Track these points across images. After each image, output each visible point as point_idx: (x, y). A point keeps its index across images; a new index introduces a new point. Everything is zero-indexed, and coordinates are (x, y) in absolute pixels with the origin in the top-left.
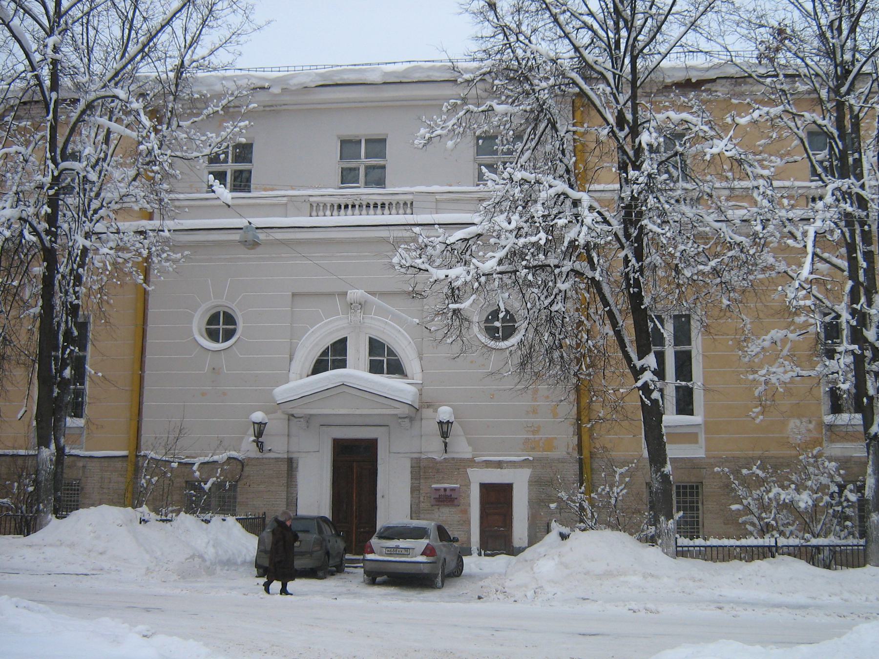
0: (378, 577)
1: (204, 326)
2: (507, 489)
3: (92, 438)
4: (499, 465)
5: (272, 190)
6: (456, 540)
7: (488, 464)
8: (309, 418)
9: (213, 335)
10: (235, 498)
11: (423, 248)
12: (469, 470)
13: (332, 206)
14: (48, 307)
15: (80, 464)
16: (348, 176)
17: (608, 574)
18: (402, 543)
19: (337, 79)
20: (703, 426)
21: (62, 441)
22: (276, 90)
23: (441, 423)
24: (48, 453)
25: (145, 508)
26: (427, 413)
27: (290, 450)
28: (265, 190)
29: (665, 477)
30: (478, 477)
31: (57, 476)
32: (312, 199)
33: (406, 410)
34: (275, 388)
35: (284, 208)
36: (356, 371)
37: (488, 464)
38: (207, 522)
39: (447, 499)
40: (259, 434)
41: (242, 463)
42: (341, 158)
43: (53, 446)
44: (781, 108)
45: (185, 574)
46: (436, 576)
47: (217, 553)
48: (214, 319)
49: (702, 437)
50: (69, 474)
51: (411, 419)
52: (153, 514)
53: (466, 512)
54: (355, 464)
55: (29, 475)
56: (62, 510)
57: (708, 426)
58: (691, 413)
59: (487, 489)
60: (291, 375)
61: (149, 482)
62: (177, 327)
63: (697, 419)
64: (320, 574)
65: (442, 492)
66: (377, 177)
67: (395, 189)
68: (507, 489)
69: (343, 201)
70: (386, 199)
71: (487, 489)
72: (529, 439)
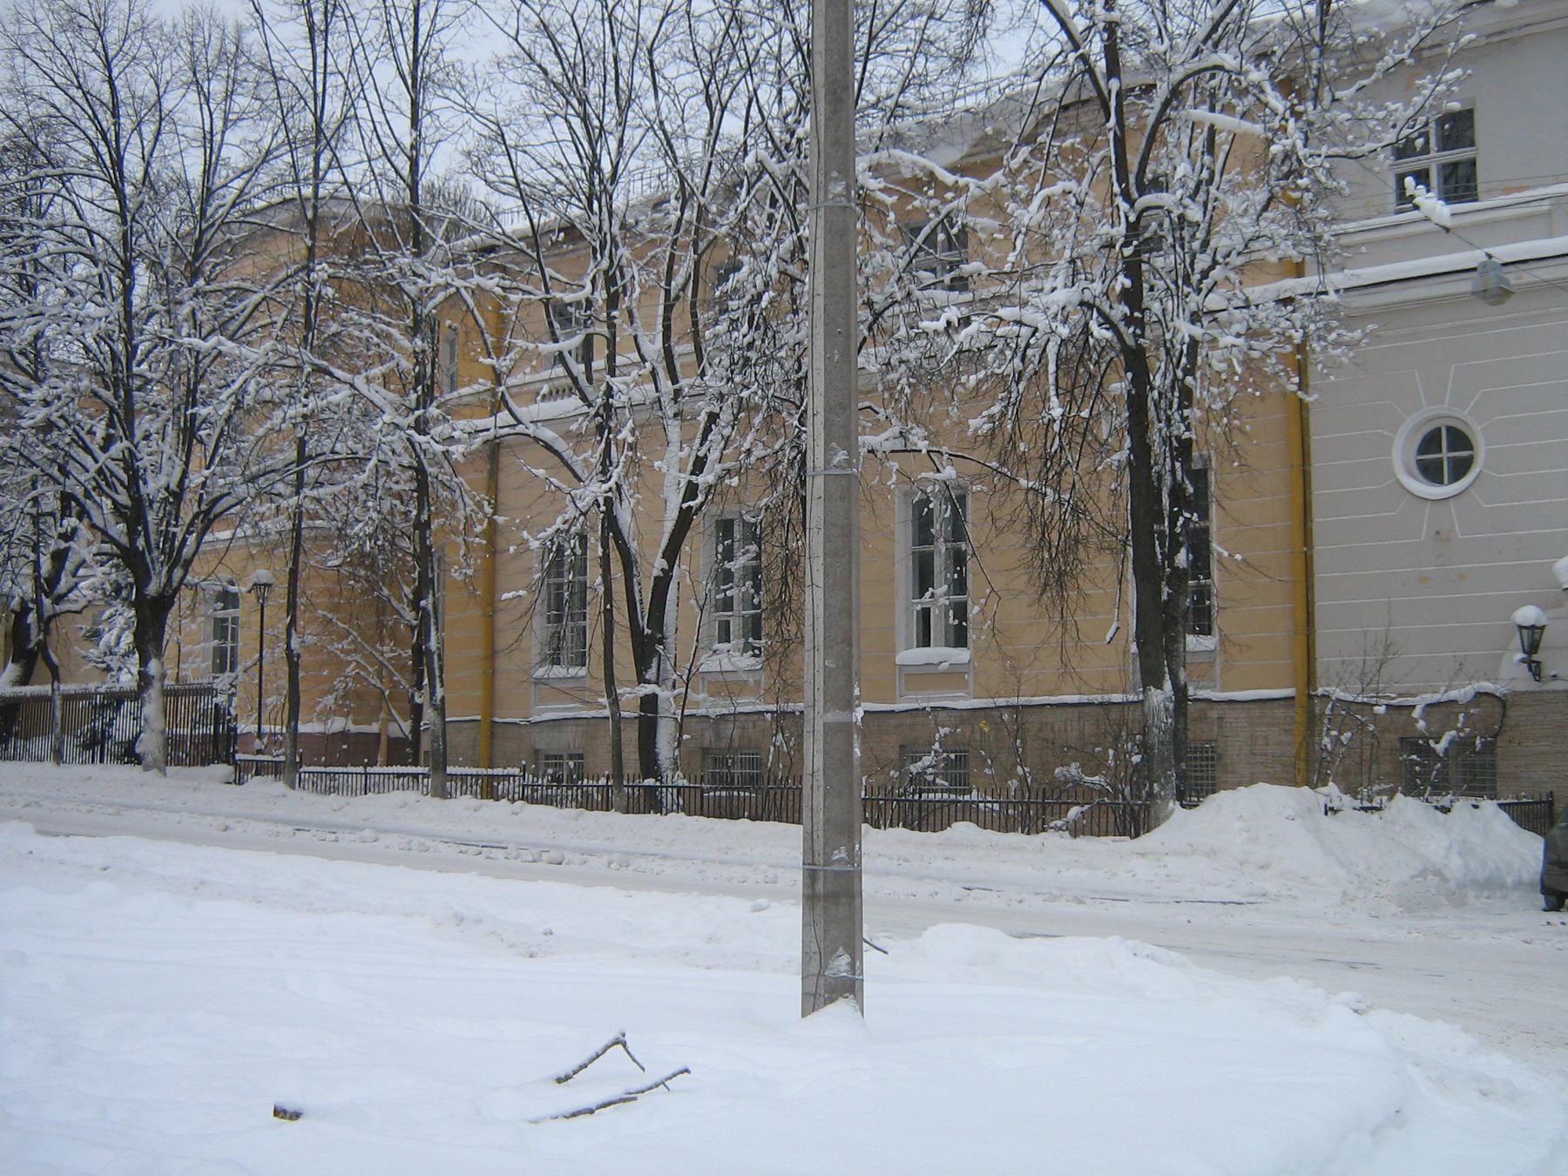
1: (1413, 457)
3: (1231, 668)
9: (1431, 472)
10: (1493, 766)
14: (1141, 449)
24: (1160, 697)
25: (1332, 788)
28: (1508, 191)
31: (1178, 736)
40: (1532, 647)
41: (1502, 702)
43: (1168, 685)
48: (1430, 442)
50: (1196, 732)
52: (1347, 798)
61: (1337, 741)
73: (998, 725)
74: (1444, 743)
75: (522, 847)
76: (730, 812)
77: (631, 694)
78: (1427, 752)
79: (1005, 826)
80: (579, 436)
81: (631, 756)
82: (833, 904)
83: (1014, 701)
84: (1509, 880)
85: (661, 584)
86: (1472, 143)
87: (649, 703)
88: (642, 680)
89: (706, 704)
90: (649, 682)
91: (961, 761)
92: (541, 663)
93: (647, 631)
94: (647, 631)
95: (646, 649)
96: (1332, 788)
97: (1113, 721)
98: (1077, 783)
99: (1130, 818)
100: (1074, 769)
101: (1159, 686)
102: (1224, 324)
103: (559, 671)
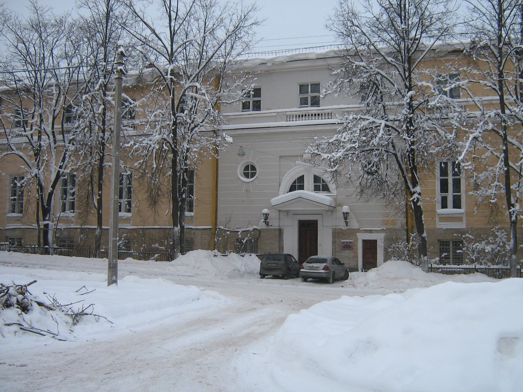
0: (305, 279)
1: (242, 171)
2: (375, 242)
3: (196, 220)
4: (371, 231)
5: (270, 109)
6: (343, 264)
7: (366, 231)
8: (287, 212)
9: (247, 175)
10: (257, 246)
11: (318, 145)
12: (357, 234)
13: (296, 116)
14: (175, 172)
15: (193, 232)
16: (304, 102)
17: (396, 278)
18: (315, 265)
19: (296, 58)
20: (465, 214)
21: (183, 223)
22: (269, 64)
23: (344, 213)
24: (177, 229)
25: (216, 251)
26: (338, 208)
27: (281, 225)
28: (267, 109)
29: (423, 239)
30: (362, 237)
31: (181, 238)
32: (287, 113)
33: (327, 208)
34: (274, 196)
35: (274, 118)
36: (307, 192)
37: (366, 231)
38: (243, 256)
39: (348, 247)
40: (266, 219)
41: (260, 231)
42: (300, 93)
43: (179, 226)
44: (467, 81)
45: (230, 277)
46: (330, 278)
47: (246, 269)
48: (247, 168)
49: (464, 219)
50: (187, 236)
51: (332, 212)
52: (219, 253)
53: (356, 252)
54: (308, 231)
55: (171, 238)
56: (183, 252)
57: (467, 214)
58: (460, 207)
59: (365, 242)
60: (280, 192)
61: (218, 240)
62: (232, 171)
63: (462, 210)
64: (286, 277)
65: (345, 244)
66: (316, 102)
67: (324, 107)
68: (375, 242)
69: (301, 114)
70: (320, 112)
71: (365, 242)
72: (384, 220)
73: (138, 234)
74: (245, 240)
75: (16, 263)
76: (69, 254)
77: (42, 223)
78: (241, 242)
79: (140, 259)
80: (31, 156)
81: (42, 241)
82: (113, 270)
83: (142, 227)
84: (256, 272)
85: (51, 194)
86: (260, 97)
87: (46, 226)
88: (44, 220)
89: (61, 226)
90: (46, 220)
91: (129, 242)
92: (9, 213)
93: (46, 207)
94: (46, 207)
95: (46, 211)
96: (216, 251)
97: (166, 233)
98: (158, 248)
99: (170, 257)
100: (157, 245)
101: (177, 227)
102: (194, 150)
103: (14, 215)
